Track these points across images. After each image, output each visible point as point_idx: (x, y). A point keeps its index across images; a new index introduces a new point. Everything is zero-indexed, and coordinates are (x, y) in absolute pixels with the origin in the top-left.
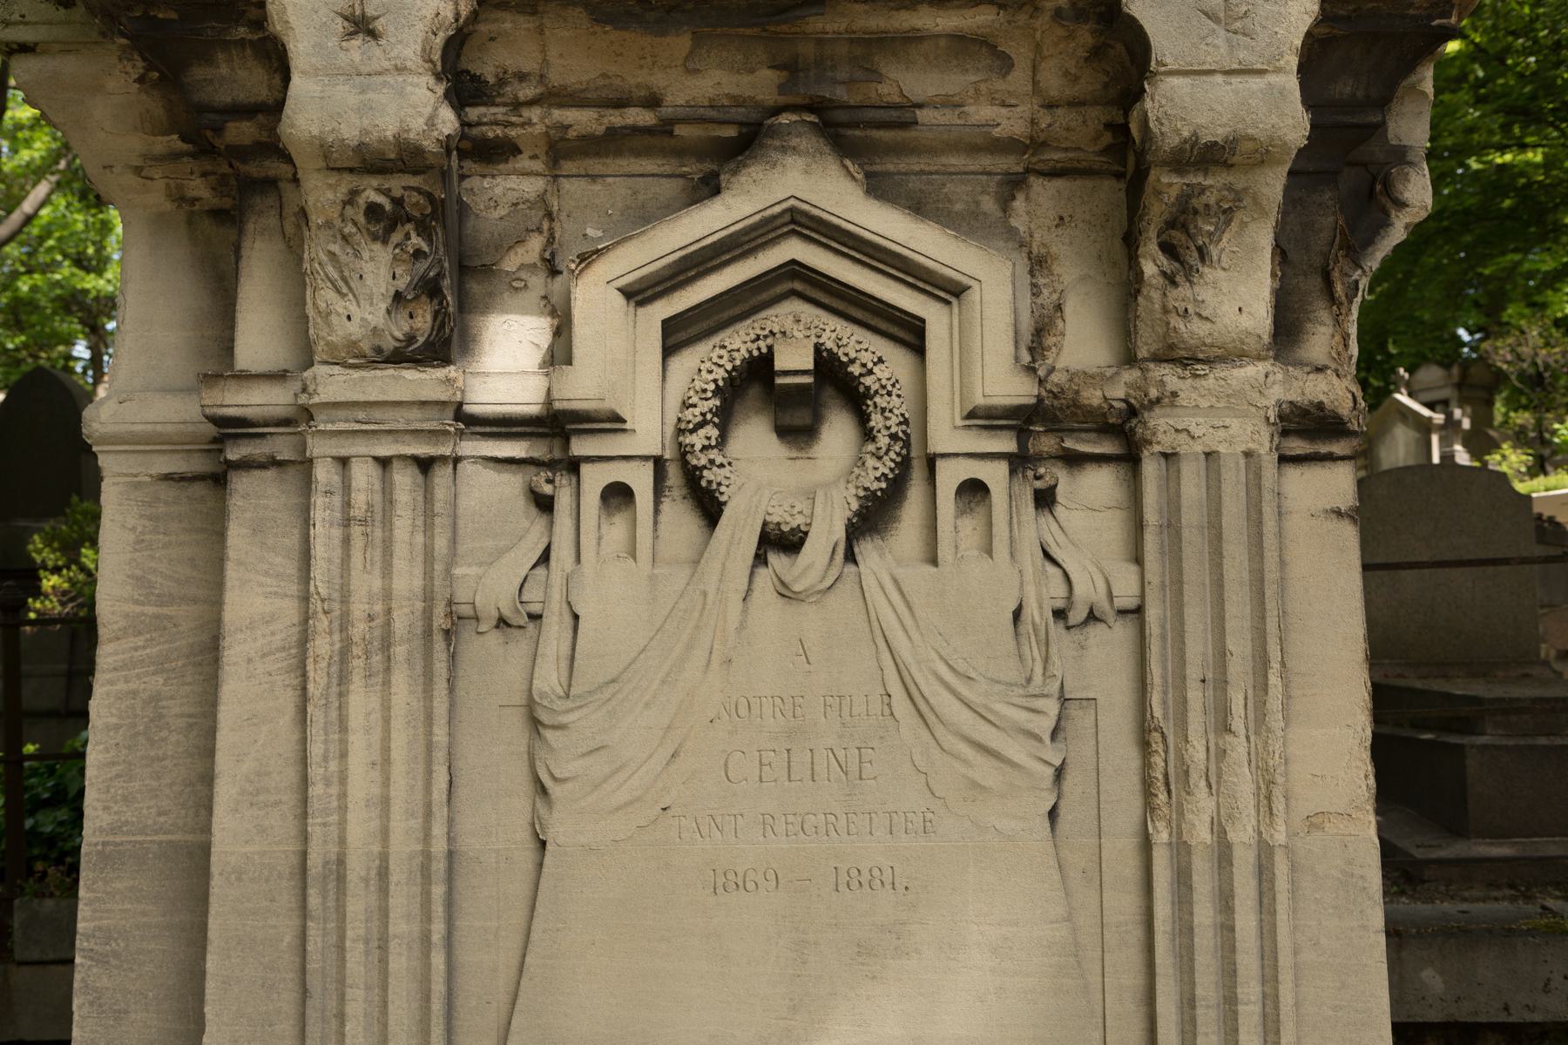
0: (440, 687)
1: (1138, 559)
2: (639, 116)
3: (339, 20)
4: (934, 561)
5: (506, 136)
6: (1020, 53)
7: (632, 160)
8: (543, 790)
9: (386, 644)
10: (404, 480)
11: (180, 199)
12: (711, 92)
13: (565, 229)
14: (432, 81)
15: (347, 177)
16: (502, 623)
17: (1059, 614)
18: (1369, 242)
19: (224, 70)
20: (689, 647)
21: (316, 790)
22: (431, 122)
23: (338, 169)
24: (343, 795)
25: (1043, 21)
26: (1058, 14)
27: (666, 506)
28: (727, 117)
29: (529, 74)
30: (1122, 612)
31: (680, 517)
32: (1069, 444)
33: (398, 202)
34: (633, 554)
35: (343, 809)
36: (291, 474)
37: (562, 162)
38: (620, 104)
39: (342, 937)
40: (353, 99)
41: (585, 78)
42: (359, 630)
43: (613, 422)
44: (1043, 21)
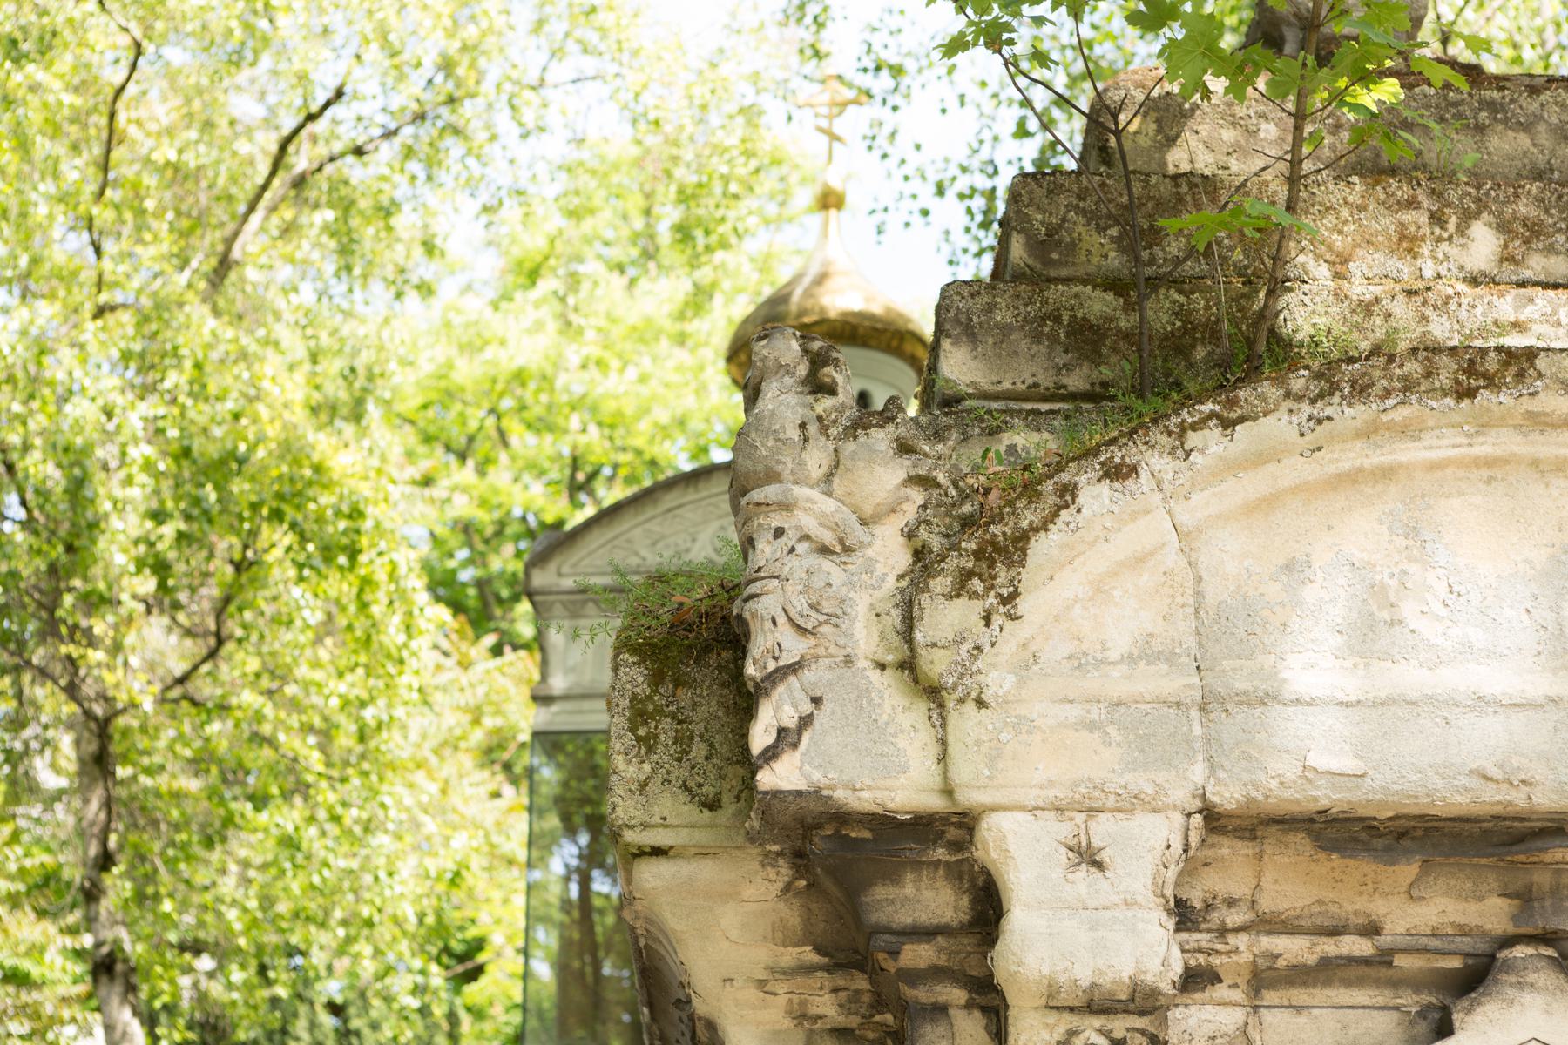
3: (1064, 850)
5: (1210, 965)
7: (1342, 990)
11: (802, 1016)
12: (1434, 920)
14: (1164, 916)
15: (1067, 1016)
19: (909, 890)
23: (1058, 1008)
28: (1452, 947)
29: (1240, 900)
37: (1264, 992)
38: (1334, 932)
41: (1299, 904)
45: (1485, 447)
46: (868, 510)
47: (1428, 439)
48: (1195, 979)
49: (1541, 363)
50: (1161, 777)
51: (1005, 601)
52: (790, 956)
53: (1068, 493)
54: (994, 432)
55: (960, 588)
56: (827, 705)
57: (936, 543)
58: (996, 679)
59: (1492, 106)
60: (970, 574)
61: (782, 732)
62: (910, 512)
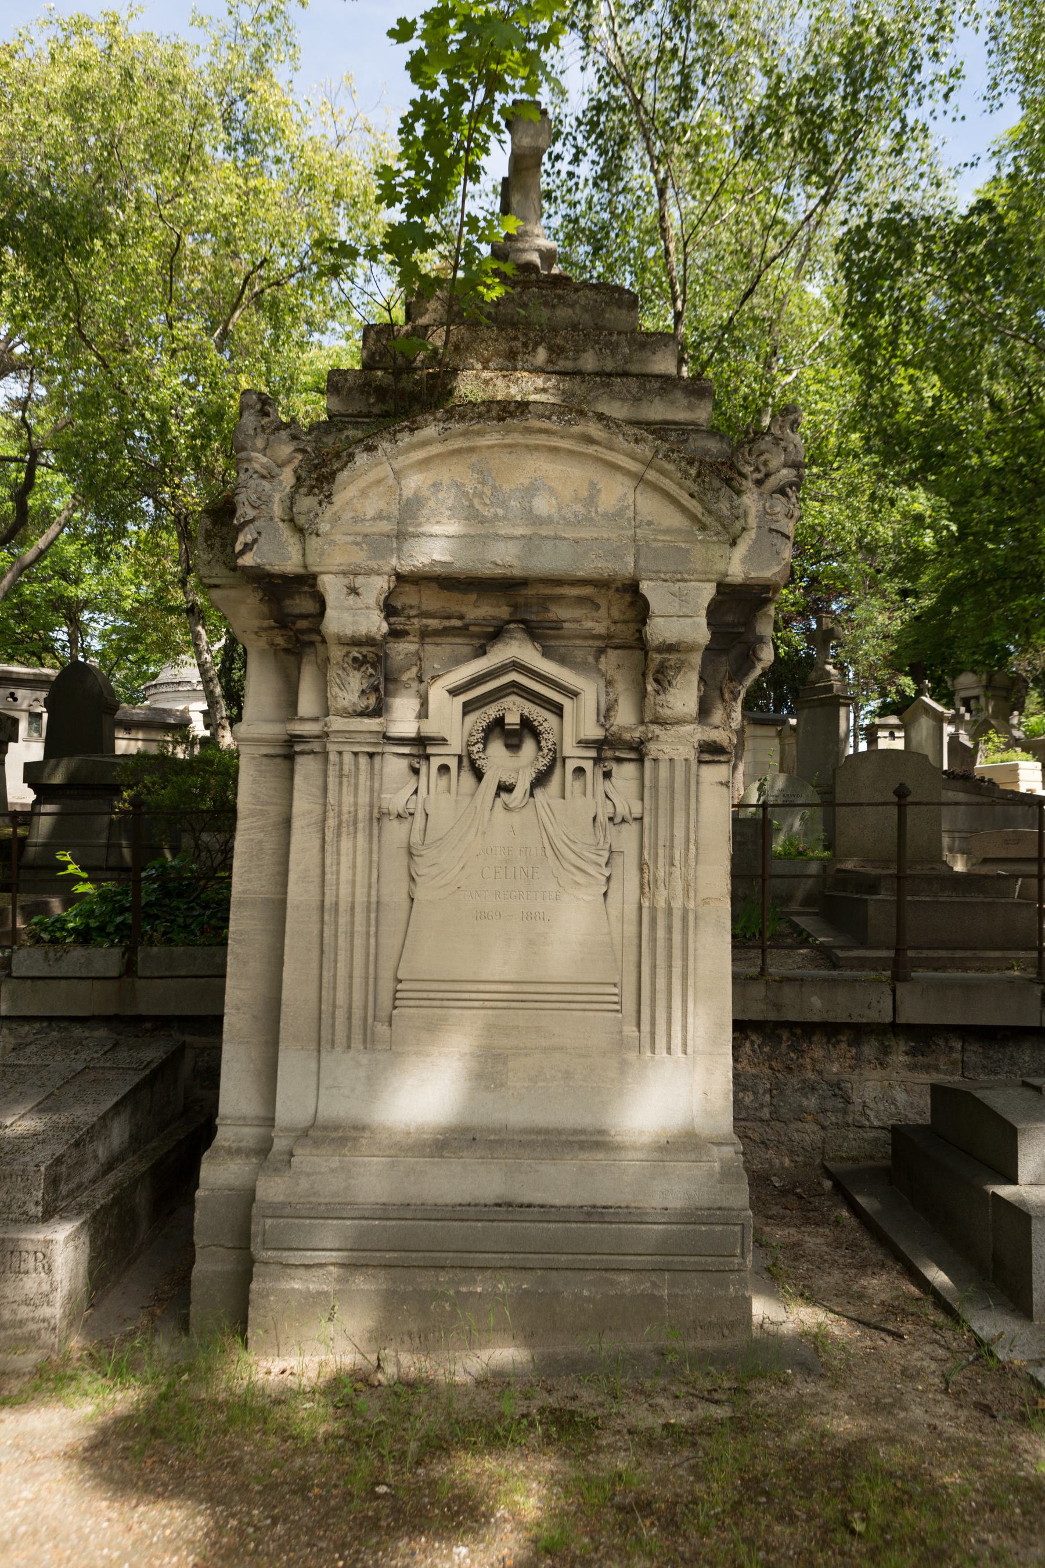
0: (375, 839)
1: (642, 800)
2: (457, 623)
4: (564, 798)
6: (603, 603)
8: (413, 879)
9: (355, 822)
10: (363, 760)
11: (272, 644)
13: (426, 664)
16: (399, 816)
17: (611, 819)
18: (746, 674)
20: (470, 827)
21: (328, 877)
22: (379, 629)
24: (338, 879)
25: (611, 592)
26: (617, 590)
27: (462, 773)
30: (635, 819)
31: (468, 778)
32: (617, 754)
33: (365, 656)
34: (449, 791)
35: (338, 884)
36: (319, 757)
38: (449, 618)
39: (337, 931)
40: (350, 619)
42: (345, 817)
43: (443, 741)
44: (611, 592)
45: (508, 441)
47: (487, 437)
48: (396, 634)
50: (381, 563)
51: (327, 497)
52: (266, 623)
53: (351, 457)
54: (341, 430)
55: (310, 493)
57: (304, 474)
58: (324, 527)
60: (314, 487)
61: (246, 545)
62: (296, 462)
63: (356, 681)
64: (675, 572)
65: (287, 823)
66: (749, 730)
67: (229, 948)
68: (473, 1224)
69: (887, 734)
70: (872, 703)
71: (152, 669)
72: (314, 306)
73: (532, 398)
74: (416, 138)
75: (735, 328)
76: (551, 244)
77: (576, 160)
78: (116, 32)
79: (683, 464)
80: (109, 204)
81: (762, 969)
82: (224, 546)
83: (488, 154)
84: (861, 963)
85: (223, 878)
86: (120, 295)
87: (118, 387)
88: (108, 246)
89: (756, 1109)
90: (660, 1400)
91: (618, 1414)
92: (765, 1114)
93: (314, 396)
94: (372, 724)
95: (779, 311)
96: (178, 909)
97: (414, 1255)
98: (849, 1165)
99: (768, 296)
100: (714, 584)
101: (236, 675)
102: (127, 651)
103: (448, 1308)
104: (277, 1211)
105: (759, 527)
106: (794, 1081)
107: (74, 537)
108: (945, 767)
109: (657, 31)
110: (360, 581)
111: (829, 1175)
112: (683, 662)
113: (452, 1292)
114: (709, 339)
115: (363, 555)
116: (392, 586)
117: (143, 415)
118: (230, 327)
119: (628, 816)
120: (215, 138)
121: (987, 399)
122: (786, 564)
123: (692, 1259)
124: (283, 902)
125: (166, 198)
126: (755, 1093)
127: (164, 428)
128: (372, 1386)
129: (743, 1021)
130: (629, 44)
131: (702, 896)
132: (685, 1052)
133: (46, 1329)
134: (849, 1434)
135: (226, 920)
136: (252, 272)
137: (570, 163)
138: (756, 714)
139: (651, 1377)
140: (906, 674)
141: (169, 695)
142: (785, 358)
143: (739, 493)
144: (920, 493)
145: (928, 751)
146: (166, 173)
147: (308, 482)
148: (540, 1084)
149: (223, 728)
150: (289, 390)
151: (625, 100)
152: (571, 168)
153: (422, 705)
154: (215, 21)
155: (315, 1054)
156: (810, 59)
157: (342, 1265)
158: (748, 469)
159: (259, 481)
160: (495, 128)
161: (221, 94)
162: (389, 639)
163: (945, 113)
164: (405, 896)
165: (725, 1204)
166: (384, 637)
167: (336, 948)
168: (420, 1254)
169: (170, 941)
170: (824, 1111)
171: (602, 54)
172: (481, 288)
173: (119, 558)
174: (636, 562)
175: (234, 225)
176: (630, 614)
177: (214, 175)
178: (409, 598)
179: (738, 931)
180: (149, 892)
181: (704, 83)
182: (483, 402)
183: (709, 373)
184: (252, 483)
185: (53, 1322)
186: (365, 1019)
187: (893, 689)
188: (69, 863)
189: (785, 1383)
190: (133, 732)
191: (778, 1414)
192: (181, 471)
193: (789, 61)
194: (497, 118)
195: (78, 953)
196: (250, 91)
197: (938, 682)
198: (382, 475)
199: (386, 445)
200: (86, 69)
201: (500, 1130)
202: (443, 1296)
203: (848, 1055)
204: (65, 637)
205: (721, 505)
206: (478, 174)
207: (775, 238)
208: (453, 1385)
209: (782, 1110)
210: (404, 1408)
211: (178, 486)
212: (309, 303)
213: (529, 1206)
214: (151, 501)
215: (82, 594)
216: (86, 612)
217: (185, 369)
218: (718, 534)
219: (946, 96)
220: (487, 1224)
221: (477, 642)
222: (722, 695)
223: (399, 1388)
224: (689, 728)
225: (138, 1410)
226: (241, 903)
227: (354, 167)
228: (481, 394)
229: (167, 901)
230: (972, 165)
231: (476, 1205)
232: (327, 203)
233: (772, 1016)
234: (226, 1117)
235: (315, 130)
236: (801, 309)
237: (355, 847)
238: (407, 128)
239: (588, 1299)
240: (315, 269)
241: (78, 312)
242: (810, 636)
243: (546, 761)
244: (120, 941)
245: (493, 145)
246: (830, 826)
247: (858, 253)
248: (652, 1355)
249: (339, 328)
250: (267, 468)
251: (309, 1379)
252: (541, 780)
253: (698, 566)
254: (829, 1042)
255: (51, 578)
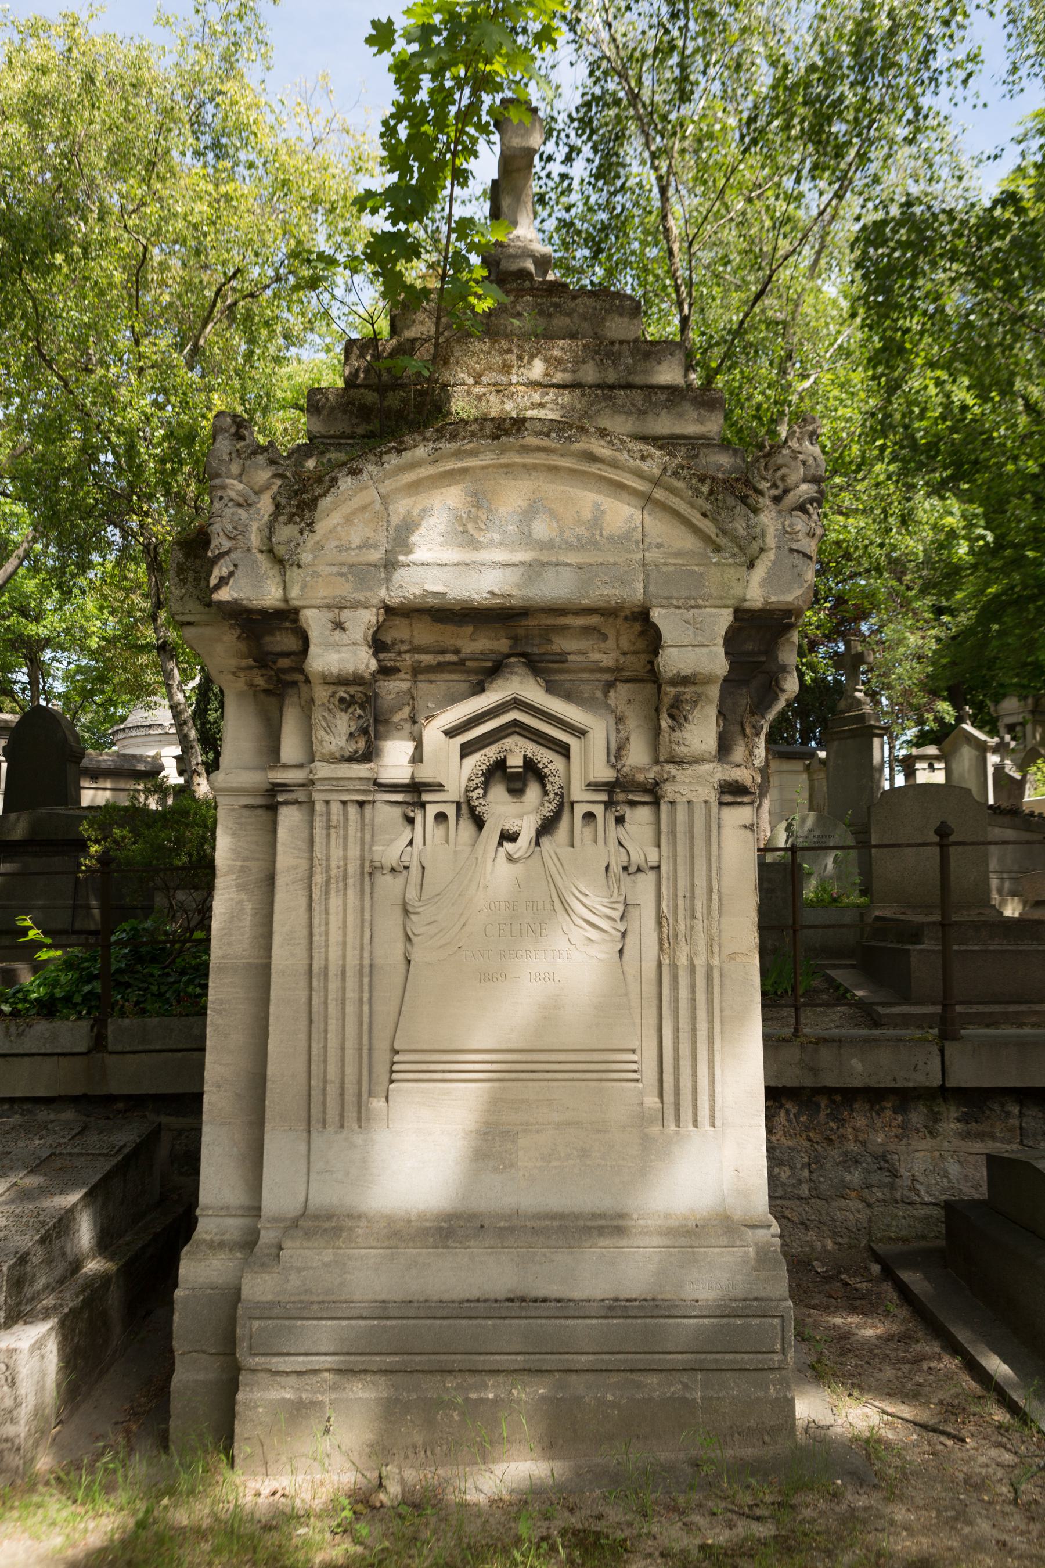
1: (659, 846)
4: (573, 846)
6: (611, 633)
9: (345, 878)
10: (353, 810)
11: (251, 685)
13: (419, 703)
16: (393, 870)
17: (625, 869)
18: (769, 707)
19: (278, 638)
21: (316, 938)
22: (367, 666)
24: (327, 941)
25: (620, 621)
26: (626, 618)
27: (461, 821)
30: (652, 868)
31: (467, 827)
32: (631, 797)
33: (352, 696)
34: (447, 842)
35: (327, 946)
38: (443, 652)
43: (439, 787)
44: (620, 621)
45: (504, 460)
46: (257, 488)
47: (481, 457)
48: (386, 671)
49: (527, 425)
50: (368, 594)
51: (308, 525)
52: (244, 663)
53: (334, 481)
54: (322, 453)
55: (290, 521)
56: (240, 568)
57: (283, 501)
58: (306, 557)
59: (556, 306)
60: (294, 514)
61: (222, 578)
62: (275, 488)
63: (343, 723)
64: (688, 598)
65: (270, 880)
66: (774, 765)
67: (209, 1019)
68: (482, 1322)
69: (925, 765)
70: (908, 732)
71: (120, 712)
72: (292, 319)
73: (530, 413)
74: (399, 141)
75: (746, 332)
76: (548, 249)
77: (568, 159)
78: (76, 34)
79: (694, 481)
80: (70, 215)
81: (796, 1030)
82: (197, 580)
83: (476, 157)
84: (906, 1021)
85: (201, 941)
86: (83, 311)
87: (81, 408)
88: (69, 259)
89: (794, 1186)
90: (696, 1518)
91: (648, 1535)
92: (804, 1190)
93: (293, 413)
94: (361, 770)
95: (794, 313)
96: (152, 975)
97: (418, 1358)
98: (899, 1247)
99: (780, 297)
100: (731, 610)
101: (212, 716)
102: (92, 693)
103: (457, 1418)
104: (265, 1311)
105: (778, 548)
106: (835, 1154)
107: (35, 570)
108: (991, 801)
109: (655, 20)
110: (346, 615)
111: (877, 1258)
112: (699, 695)
113: (460, 1400)
114: (717, 344)
115: (349, 586)
116: (381, 619)
117: (108, 439)
118: (202, 342)
119: (643, 865)
120: (184, 144)
121: (1020, 401)
122: (809, 587)
123: (728, 1357)
124: (268, 966)
125: (131, 208)
126: (792, 1168)
127: (131, 449)
128: (373, 1508)
129: (776, 1088)
130: (624, 35)
131: (726, 951)
132: (713, 1125)
133: (10, 1450)
134: (908, 1553)
135: (205, 987)
136: (224, 284)
137: (562, 162)
138: (784, 748)
139: (684, 1492)
140: (945, 699)
141: (139, 740)
142: (801, 362)
143: (756, 511)
144: (955, 505)
145: (972, 784)
146: (131, 181)
147: (288, 510)
148: (554, 1163)
149: (199, 775)
150: (265, 411)
151: (622, 94)
152: (563, 169)
153: (416, 748)
154: (181, 20)
155: (305, 1134)
156: (817, 47)
157: (339, 1371)
158: (764, 485)
159: (234, 510)
160: (483, 129)
161: (190, 97)
162: (379, 677)
163: (965, 99)
164: (401, 958)
165: (763, 1294)
166: (373, 675)
167: (326, 1017)
168: (425, 1358)
169: (144, 1011)
170: (869, 1186)
171: (595, 46)
172: (472, 299)
173: (84, 592)
174: (645, 588)
175: (205, 235)
176: (641, 644)
177: (182, 182)
178: (399, 632)
179: (769, 988)
180: (119, 957)
181: (704, 73)
182: (476, 420)
183: (720, 381)
184: (228, 512)
185: (17, 1441)
186: (359, 1095)
187: (931, 716)
188: (30, 928)
189: (835, 1495)
190: (101, 780)
191: (827, 1531)
192: (150, 497)
193: (797, 48)
194: (485, 118)
195: (41, 1027)
196: (221, 93)
197: (979, 707)
198: (368, 500)
199: (371, 468)
200: (44, 73)
201: (510, 1216)
202: (451, 1405)
203: (894, 1123)
204: (25, 679)
205: (736, 525)
206: (466, 179)
207: (785, 237)
208: (464, 1505)
209: (823, 1187)
210: (409, 1532)
211: (147, 514)
212: (286, 315)
213: (545, 1300)
214: (117, 531)
215: (43, 632)
216: (48, 651)
217: (153, 389)
218: (734, 555)
219: (965, 82)
220: (498, 1321)
221: (474, 679)
222: (743, 730)
223: (404, 1510)
224: (708, 767)
225: (111, 1540)
226: (220, 969)
227: (332, 170)
228: (473, 411)
229: (139, 967)
230: (996, 157)
231: (486, 1301)
232: (304, 208)
233: (809, 1082)
234: (207, 1208)
235: (290, 132)
236: (817, 311)
237: (345, 904)
238: (389, 131)
239: (613, 1405)
240: (292, 280)
241: (38, 330)
242: (837, 659)
243: (553, 806)
244: (88, 1013)
245: (482, 146)
246: (866, 869)
247: (876, 250)
248: (685, 1466)
249: (318, 340)
250: (243, 496)
251: (303, 1501)
252: (547, 827)
253: (713, 591)
254: (872, 1109)
255: (11, 615)
